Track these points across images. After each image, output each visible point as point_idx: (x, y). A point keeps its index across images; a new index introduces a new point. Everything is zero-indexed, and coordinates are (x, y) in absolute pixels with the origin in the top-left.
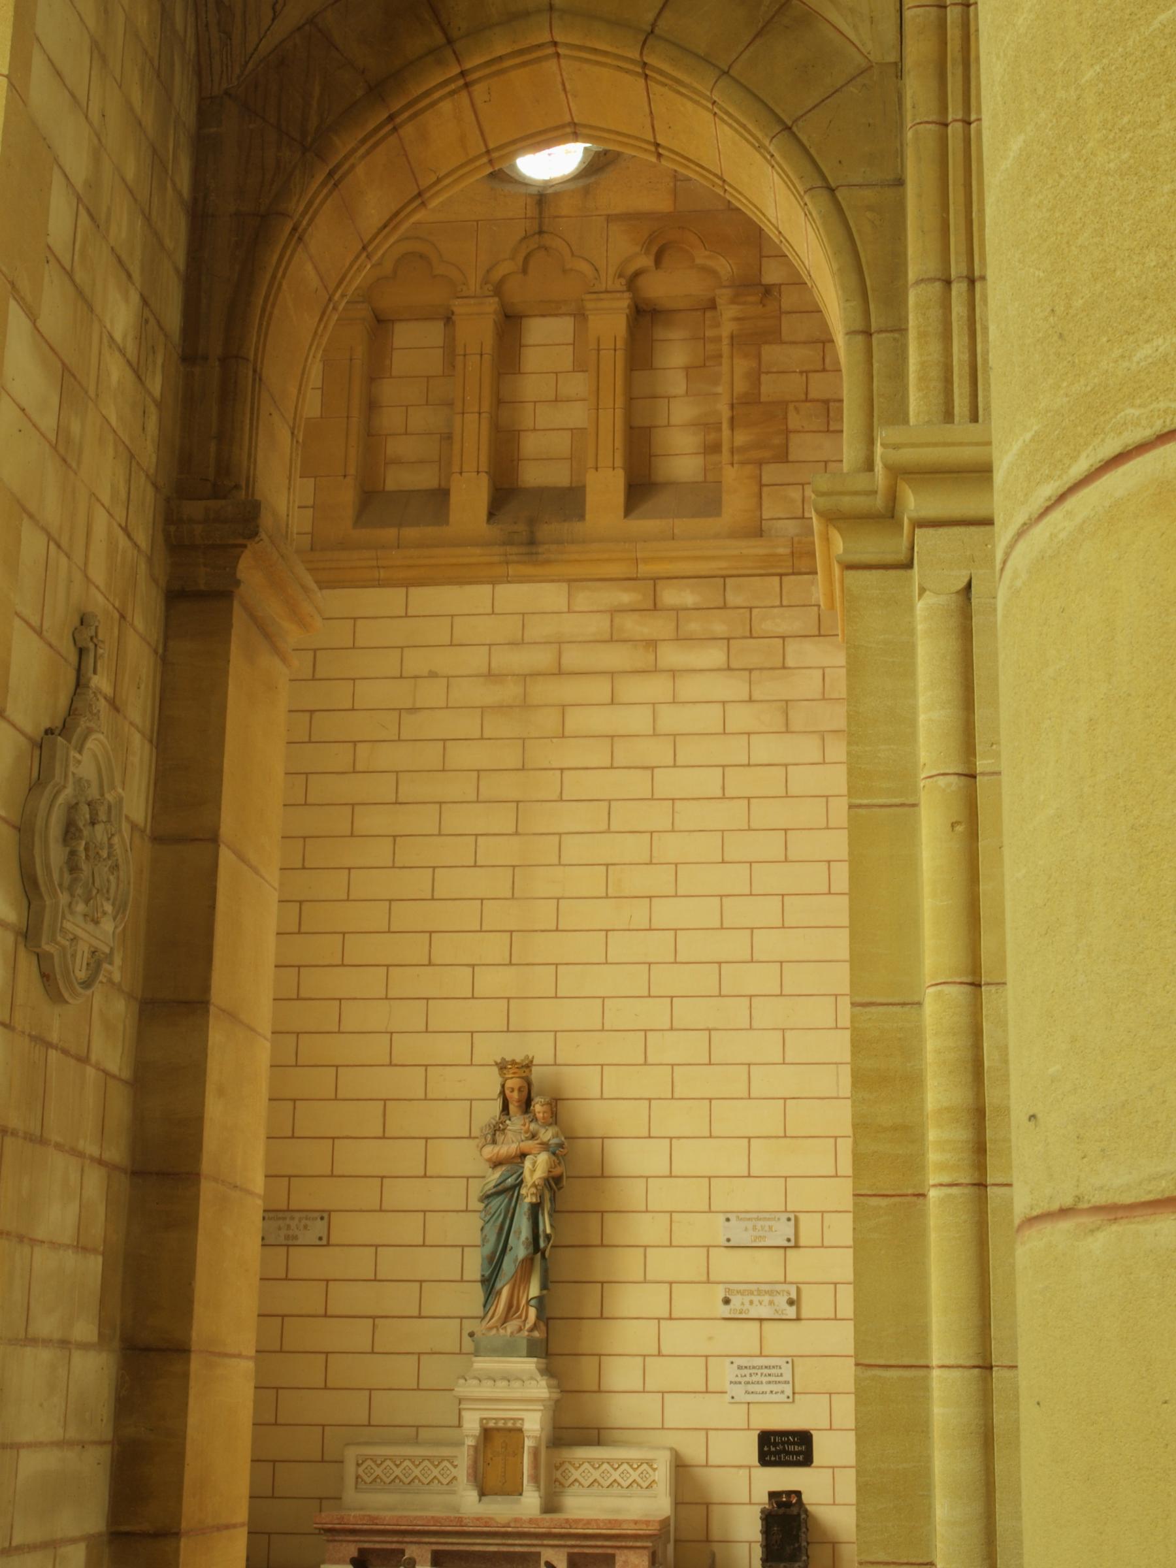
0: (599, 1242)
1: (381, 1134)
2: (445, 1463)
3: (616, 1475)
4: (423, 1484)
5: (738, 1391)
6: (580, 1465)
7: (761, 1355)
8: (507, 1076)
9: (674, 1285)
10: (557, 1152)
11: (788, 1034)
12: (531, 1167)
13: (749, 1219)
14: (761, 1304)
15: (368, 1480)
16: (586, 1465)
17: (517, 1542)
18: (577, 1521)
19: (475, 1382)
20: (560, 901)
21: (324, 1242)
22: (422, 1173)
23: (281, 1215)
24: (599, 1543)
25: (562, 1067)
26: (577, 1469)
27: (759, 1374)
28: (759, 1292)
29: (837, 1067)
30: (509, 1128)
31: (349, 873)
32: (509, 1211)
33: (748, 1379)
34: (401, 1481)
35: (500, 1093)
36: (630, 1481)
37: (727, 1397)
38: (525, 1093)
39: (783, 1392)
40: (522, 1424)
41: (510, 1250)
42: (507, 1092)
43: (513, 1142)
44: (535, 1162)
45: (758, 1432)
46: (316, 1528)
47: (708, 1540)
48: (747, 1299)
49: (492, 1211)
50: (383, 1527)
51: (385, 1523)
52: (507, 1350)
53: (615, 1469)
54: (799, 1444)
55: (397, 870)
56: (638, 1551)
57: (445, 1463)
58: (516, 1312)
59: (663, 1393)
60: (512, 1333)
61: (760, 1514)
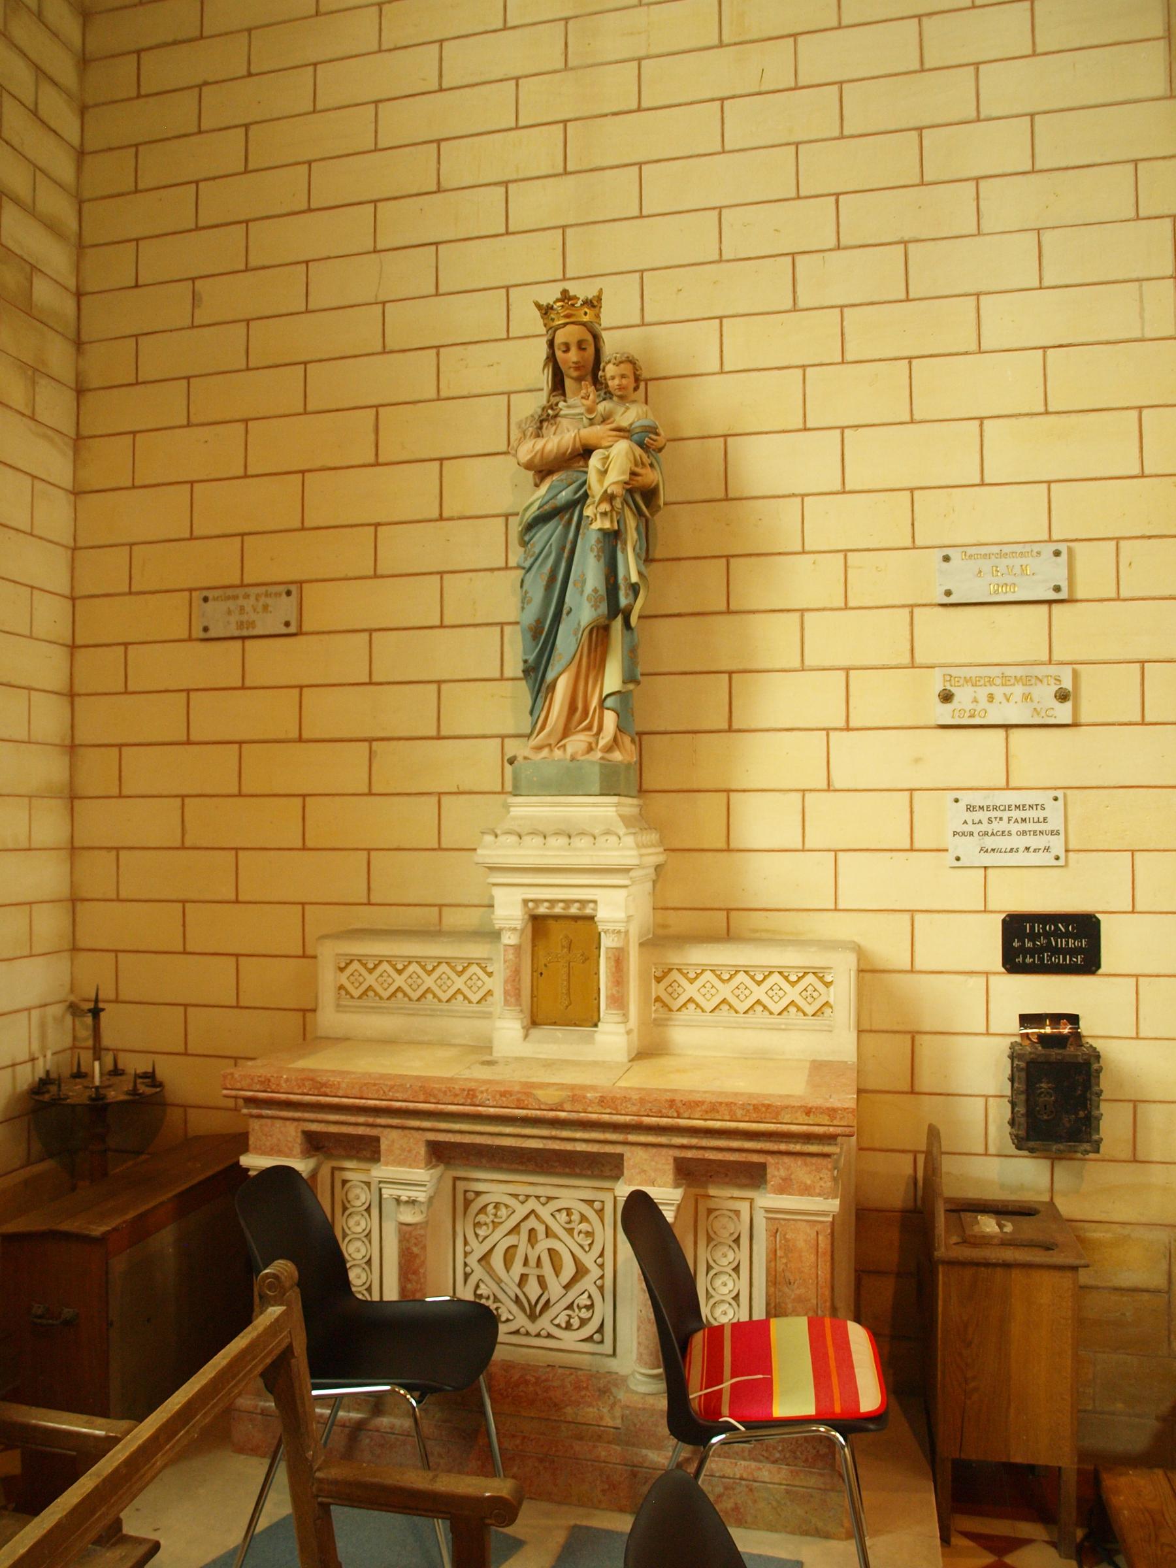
2: (474, 969)
3: (759, 993)
4: (440, 1001)
5: (968, 848)
6: (698, 976)
9: (852, 673)
11: (1047, 237)
12: (599, 466)
14: (1008, 700)
15: (356, 993)
16: (708, 975)
19: (513, 839)
20: (644, 63)
21: (293, 629)
23: (229, 592)
27: (1005, 819)
28: (1006, 681)
29: (1141, 286)
30: (562, 413)
31: (315, 71)
33: (985, 827)
34: (405, 995)
35: (547, 358)
37: (949, 858)
38: (591, 350)
39: (1047, 849)
40: (595, 910)
41: (568, 613)
43: (568, 431)
44: (607, 457)
45: (1003, 916)
46: (226, 1096)
48: (982, 693)
50: (336, 1100)
51: (340, 1093)
53: (759, 983)
54: (1075, 937)
55: (387, 55)
56: (814, 1160)
57: (474, 969)
58: (580, 723)
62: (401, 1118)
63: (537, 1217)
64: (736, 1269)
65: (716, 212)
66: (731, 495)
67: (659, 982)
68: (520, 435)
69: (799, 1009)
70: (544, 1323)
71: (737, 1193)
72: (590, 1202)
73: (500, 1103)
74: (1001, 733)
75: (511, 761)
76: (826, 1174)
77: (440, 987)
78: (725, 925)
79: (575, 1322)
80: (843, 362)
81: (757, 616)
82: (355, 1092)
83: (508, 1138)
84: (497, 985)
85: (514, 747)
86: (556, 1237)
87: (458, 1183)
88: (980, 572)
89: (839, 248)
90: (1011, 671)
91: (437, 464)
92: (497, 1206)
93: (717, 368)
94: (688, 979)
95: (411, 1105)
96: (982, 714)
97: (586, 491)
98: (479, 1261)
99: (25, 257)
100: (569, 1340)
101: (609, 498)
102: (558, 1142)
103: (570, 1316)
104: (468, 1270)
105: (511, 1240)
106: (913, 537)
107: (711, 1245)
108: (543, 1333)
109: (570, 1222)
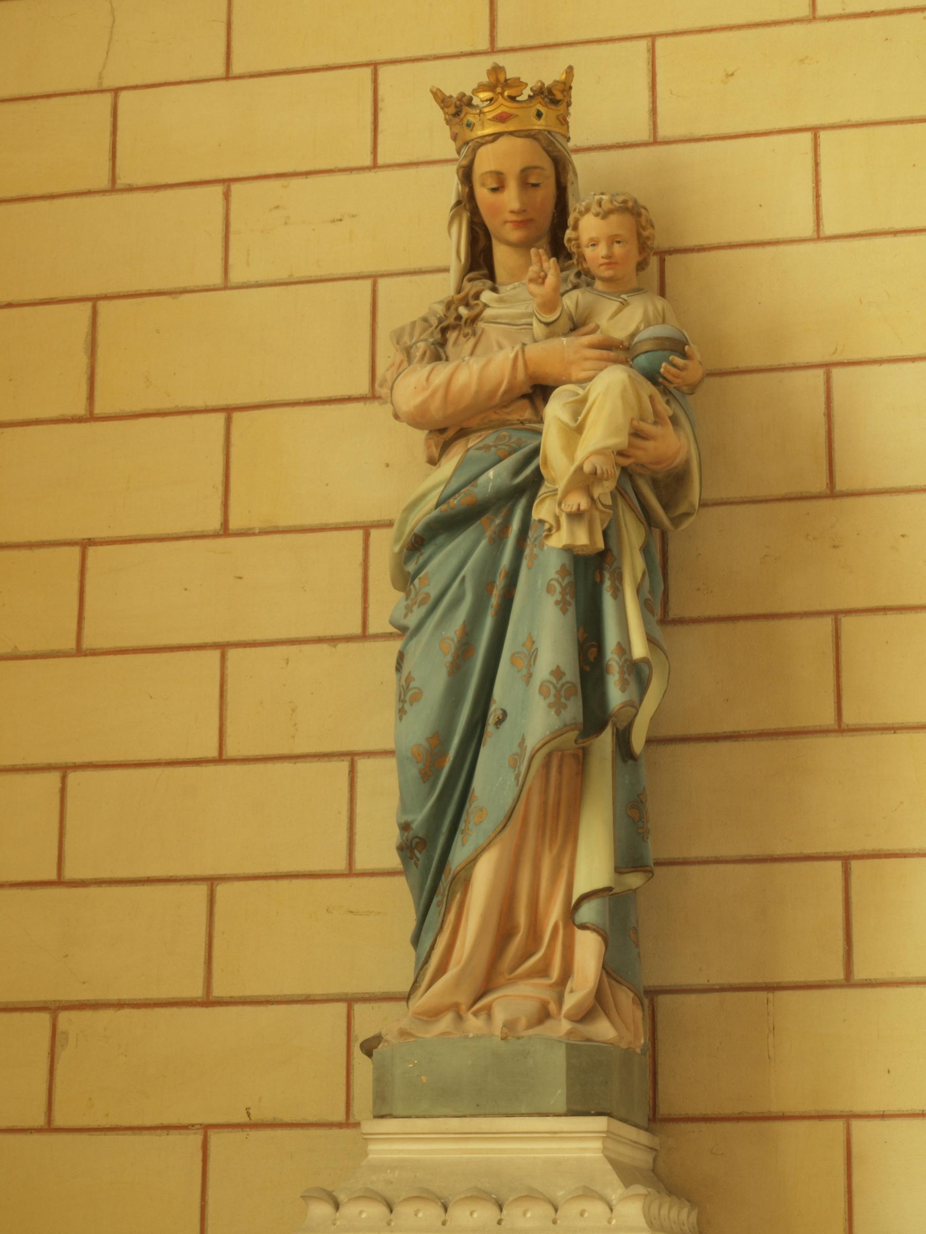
0: (828, 718)
8: (480, 132)
12: (566, 417)
30: (488, 313)
32: (491, 585)
38: (548, 191)
41: (499, 722)
42: (482, 194)
43: (501, 347)
44: (583, 401)
58: (527, 955)
60: (510, 1025)
75: (369, 1048)
93: (808, 230)
97: (537, 470)
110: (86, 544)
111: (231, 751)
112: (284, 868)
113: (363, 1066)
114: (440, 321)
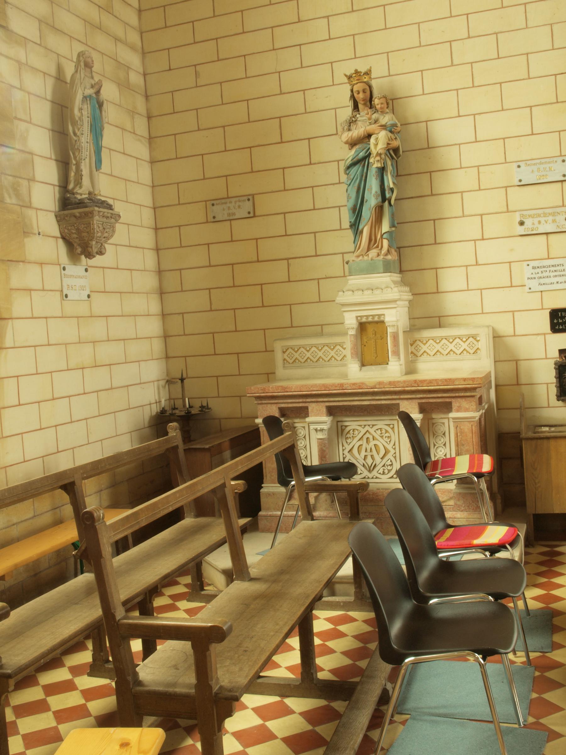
0: (430, 193)
1: (280, 141)
2: (338, 347)
3: (451, 347)
5: (534, 284)
6: (427, 342)
7: (549, 258)
10: (393, 130)
11: (555, 27)
12: (374, 142)
13: (534, 164)
14: (546, 223)
16: (431, 341)
17: (382, 398)
18: (423, 381)
19: (351, 293)
21: (252, 215)
22: (308, 162)
23: (223, 201)
24: (440, 395)
25: (393, 77)
26: (425, 344)
27: (548, 271)
28: (545, 215)
30: (358, 119)
33: (540, 275)
34: (311, 360)
35: (351, 96)
36: (462, 349)
38: (368, 92)
40: (384, 318)
41: (366, 202)
42: (355, 95)
43: (362, 127)
44: (377, 138)
45: (549, 310)
47: (518, 384)
48: (536, 220)
49: (352, 177)
51: (293, 390)
52: (370, 269)
53: (451, 343)
56: (469, 399)
57: (338, 347)
59: (481, 289)
61: (554, 366)
62: (316, 398)
63: (369, 433)
64: (445, 445)
65: (417, 25)
66: (430, 146)
67: (412, 346)
68: (342, 130)
69: (467, 352)
70: (374, 473)
71: (443, 416)
72: (389, 425)
73: (353, 388)
74: (545, 236)
75: (347, 263)
76: (473, 403)
77: (325, 356)
78: (438, 323)
79: (386, 471)
80: (473, 87)
81: (444, 196)
82: (299, 389)
83: (356, 402)
84: (348, 352)
85: (347, 257)
86: (377, 440)
87: (338, 423)
88: (533, 171)
89: (469, 37)
90: (547, 211)
91: (307, 141)
92: (354, 430)
93: (421, 93)
94: (423, 343)
95: (320, 392)
96: (537, 229)
97: (370, 152)
98: (349, 452)
99: (125, 64)
100: (384, 478)
101: (379, 155)
102: (375, 401)
103: (384, 469)
104: (344, 456)
105: (360, 443)
106: (505, 158)
107: (435, 436)
108: (374, 477)
109: (381, 434)
110: (284, 168)
111: (316, 207)
112: (328, 229)
113: (346, 266)
114: (349, 121)
